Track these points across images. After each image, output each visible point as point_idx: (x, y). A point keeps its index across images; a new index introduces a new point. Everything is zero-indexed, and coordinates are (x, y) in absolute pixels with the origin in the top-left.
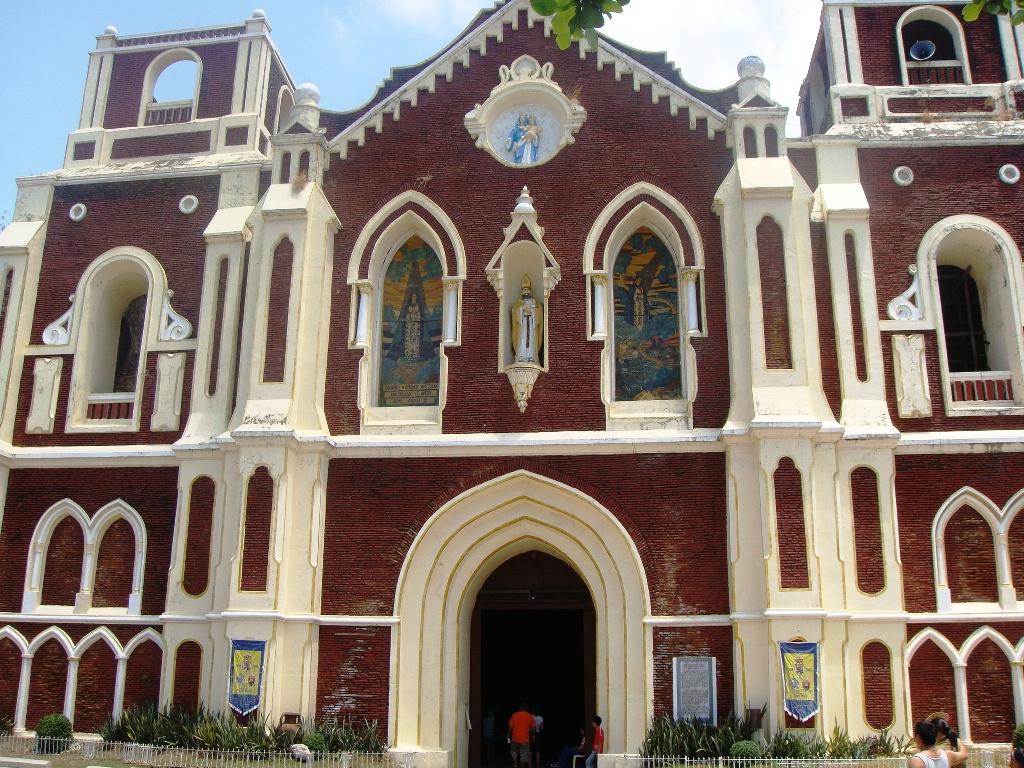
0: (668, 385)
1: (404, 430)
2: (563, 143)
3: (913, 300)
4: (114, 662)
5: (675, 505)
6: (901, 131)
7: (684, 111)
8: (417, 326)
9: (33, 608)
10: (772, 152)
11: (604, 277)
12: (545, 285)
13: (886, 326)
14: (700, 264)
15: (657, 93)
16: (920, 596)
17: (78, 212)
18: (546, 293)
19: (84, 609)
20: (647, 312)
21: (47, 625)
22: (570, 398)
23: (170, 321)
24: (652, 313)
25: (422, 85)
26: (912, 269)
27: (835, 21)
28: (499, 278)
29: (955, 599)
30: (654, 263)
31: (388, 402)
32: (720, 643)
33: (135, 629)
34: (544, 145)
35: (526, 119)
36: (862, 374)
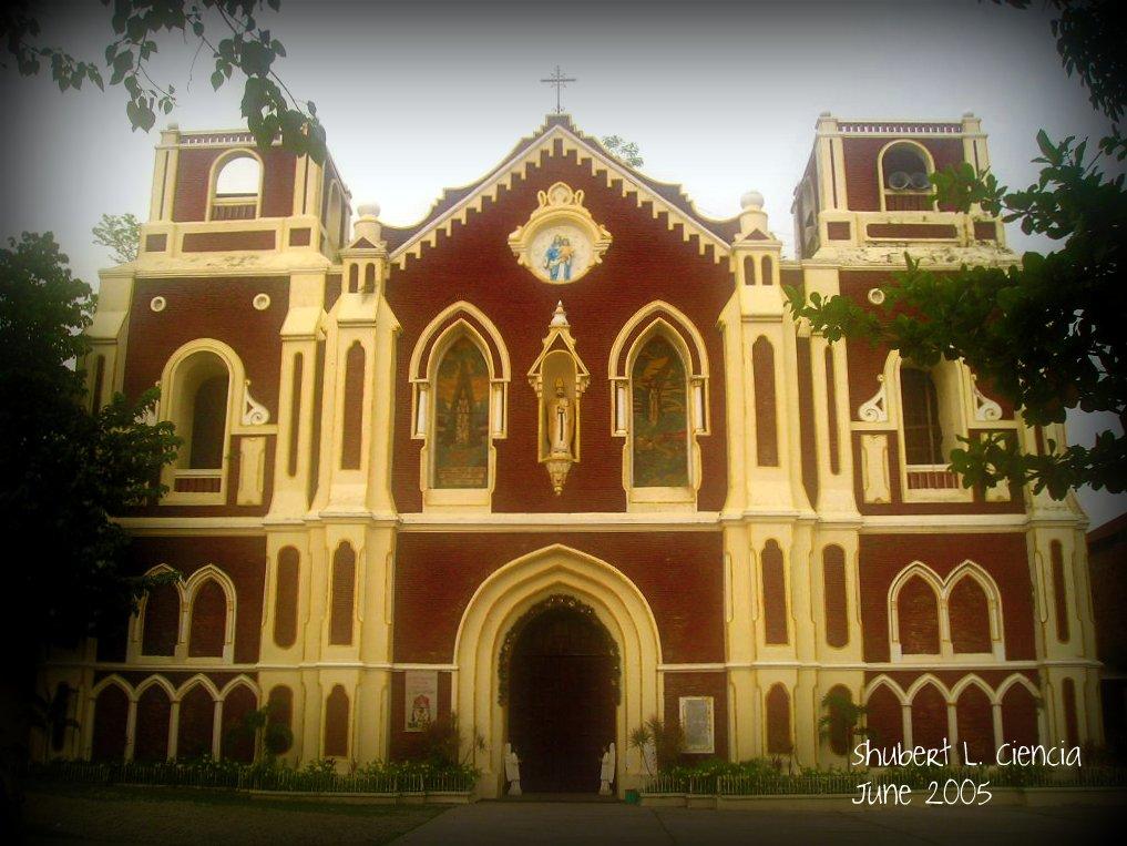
0: (674, 474)
1: (461, 508)
2: (592, 263)
3: (879, 404)
4: (212, 704)
5: (681, 577)
6: (879, 256)
7: (695, 238)
8: (466, 417)
9: (137, 659)
10: (767, 281)
11: (626, 382)
12: (577, 388)
13: (858, 426)
14: (705, 373)
15: (672, 221)
16: (876, 648)
17: (158, 304)
18: (578, 395)
19: (182, 660)
20: (660, 409)
21: (192, 674)
22: (597, 480)
23: (980, 404)
24: (664, 410)
25: (471, 205)
26: (880, 378)
27: (824, 147)
28: (538, 383)
29: (904, 652)
30: (665, 370)
31: (444, 482)
32: (716, 686)
33: (230, 675)
34: (576, 262)
35: (562, 245)
36: (835, 469)
